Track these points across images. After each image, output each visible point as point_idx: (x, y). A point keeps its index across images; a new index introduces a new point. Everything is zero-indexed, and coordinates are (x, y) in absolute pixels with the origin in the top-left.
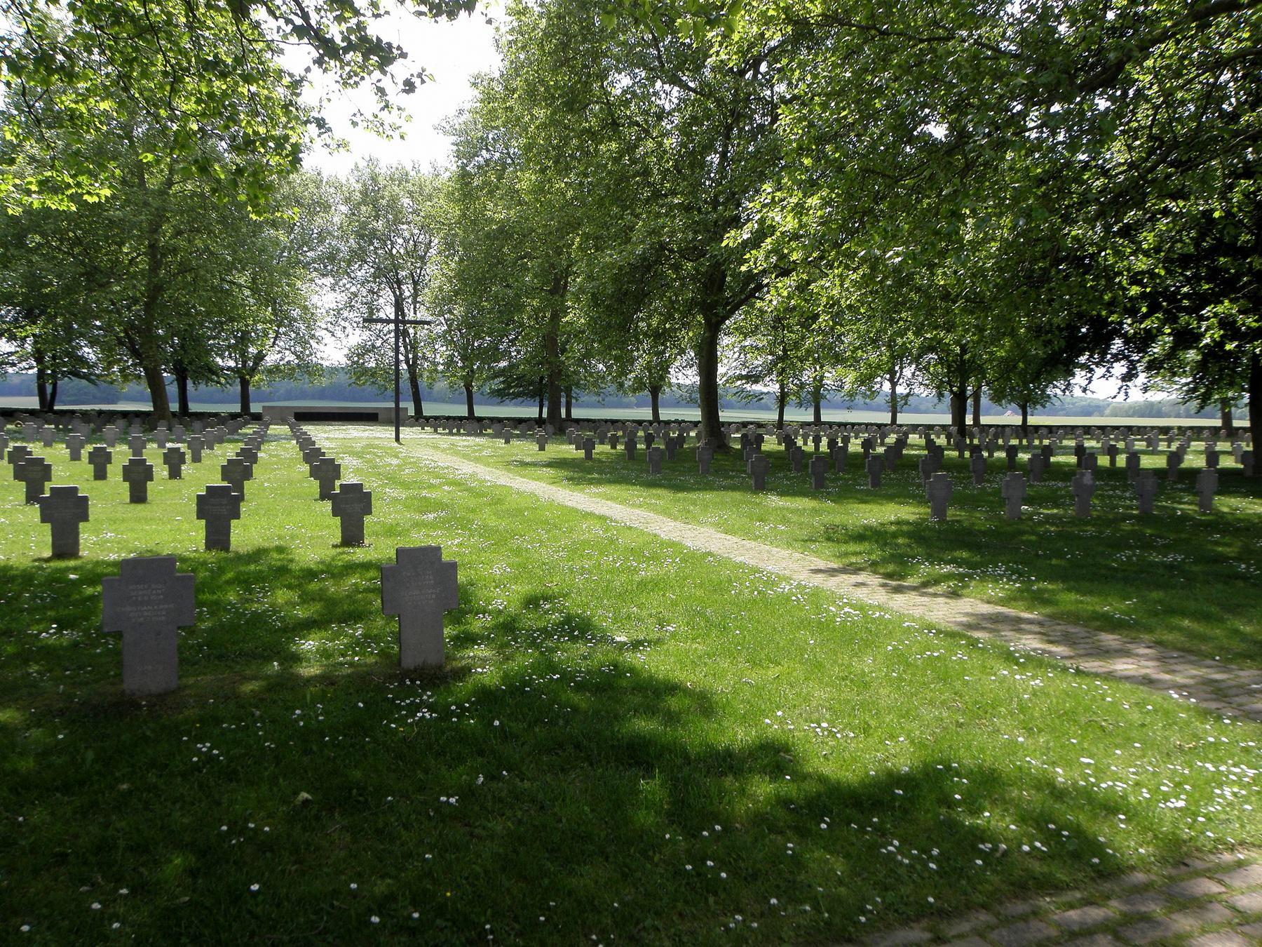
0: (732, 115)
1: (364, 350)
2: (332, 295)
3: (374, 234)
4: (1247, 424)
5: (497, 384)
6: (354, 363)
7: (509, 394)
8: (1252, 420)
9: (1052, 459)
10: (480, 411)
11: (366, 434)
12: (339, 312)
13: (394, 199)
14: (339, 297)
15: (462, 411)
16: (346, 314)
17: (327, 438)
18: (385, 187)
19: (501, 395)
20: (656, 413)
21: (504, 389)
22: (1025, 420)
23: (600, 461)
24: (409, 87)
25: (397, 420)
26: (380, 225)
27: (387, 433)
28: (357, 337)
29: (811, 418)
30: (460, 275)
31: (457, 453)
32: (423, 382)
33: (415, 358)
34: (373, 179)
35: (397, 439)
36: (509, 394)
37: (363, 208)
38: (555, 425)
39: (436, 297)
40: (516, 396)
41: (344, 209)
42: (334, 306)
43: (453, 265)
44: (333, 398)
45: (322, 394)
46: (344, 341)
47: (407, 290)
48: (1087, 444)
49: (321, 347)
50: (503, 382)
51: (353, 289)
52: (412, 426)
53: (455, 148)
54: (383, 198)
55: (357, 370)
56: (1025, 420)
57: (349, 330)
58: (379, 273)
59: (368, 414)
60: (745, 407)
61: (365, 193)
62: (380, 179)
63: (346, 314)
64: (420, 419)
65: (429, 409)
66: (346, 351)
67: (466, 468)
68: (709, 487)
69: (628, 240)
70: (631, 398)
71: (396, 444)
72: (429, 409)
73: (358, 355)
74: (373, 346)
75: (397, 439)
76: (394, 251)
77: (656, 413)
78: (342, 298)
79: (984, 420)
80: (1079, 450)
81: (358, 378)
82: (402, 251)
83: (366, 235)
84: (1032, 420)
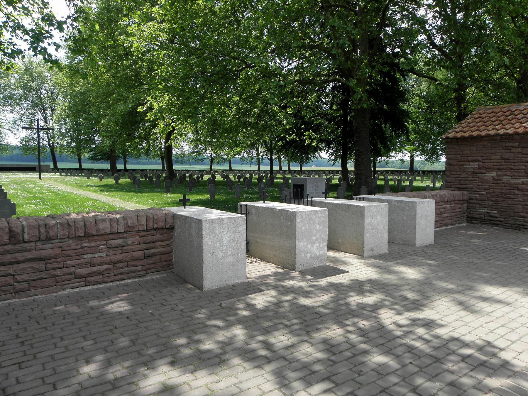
0: (354, 4)
1: (27, 139)
2: (11, 115)
3: (30, 89)
4: (353, 169)
5: (90, 155)
6: (23, 145)
7: (96, 159)
8: (355, 167)
9: (275, 180)
10: (85, 166)
11: (27, 176)
12: (15, 122)
13: (40, 73)
14: (15, 116)
15: (77, 166)
16: (19, 123)
17: (7, 178)
18: (36, 67)
19: (93, 159)
20: (125, 166)
21: (94, 157)
22: (301, 168)
23: (121, 184)
24: (63, 17)
25: (39, 169)
26: (34, 84)
27: (35, 175)
28: (24, 133)
29: (161, 168)
30: (69, 109)
31: (66, 184)
32: (57, 154)
33: (53, 143)
34: (30, 63)
35: (40, 178)
36: (96, 159)
37: (25, 77)
38: (113, 171)
39: (59, 118)
40: (100, 159)
41: (16, 76)
42: (12, 119)
43: (66, 104)
44: (17, 160)
45: (11, 159)
46: (18, 135)
47: (49, 113)
48: (287, 176)
49: (7, 138)
50: (94, 154)
51: (22, 112)
52: (51, 173)
53: (66, 55)
54: (35, 73)
55: (25, 148)
56: (301, 168)
57: (21, 129)
58: (34, 105)
59: (21, 168)
60: (198, 163)
61: (26, 70)
62: (34, 63)
63: (19, 123)
64: (56, 170)
65: (60, 165)
66: (19, 140)
67: (69, 189)
68: (152, 192)
69: (126, 102)
70: (153, 160)
71: (39, 180)
72: (60, 165)
73: (25, 142)
74: (33, 138)
75: (40, 178)
76: (42, 96)
77: (125, 166)
78: (17, 116)
79: (377, 169)
80: (284, 178)
81: (26, 152)
82: (46, 96)
83: (26, 88)
84: (304, 169)
